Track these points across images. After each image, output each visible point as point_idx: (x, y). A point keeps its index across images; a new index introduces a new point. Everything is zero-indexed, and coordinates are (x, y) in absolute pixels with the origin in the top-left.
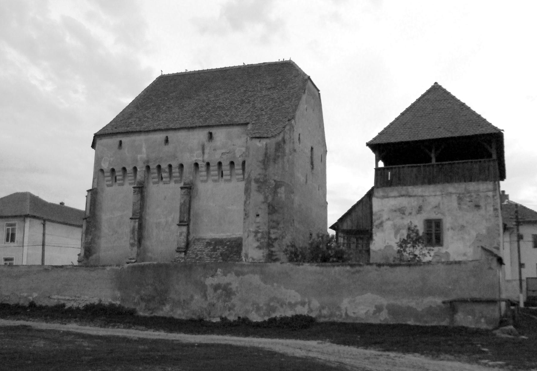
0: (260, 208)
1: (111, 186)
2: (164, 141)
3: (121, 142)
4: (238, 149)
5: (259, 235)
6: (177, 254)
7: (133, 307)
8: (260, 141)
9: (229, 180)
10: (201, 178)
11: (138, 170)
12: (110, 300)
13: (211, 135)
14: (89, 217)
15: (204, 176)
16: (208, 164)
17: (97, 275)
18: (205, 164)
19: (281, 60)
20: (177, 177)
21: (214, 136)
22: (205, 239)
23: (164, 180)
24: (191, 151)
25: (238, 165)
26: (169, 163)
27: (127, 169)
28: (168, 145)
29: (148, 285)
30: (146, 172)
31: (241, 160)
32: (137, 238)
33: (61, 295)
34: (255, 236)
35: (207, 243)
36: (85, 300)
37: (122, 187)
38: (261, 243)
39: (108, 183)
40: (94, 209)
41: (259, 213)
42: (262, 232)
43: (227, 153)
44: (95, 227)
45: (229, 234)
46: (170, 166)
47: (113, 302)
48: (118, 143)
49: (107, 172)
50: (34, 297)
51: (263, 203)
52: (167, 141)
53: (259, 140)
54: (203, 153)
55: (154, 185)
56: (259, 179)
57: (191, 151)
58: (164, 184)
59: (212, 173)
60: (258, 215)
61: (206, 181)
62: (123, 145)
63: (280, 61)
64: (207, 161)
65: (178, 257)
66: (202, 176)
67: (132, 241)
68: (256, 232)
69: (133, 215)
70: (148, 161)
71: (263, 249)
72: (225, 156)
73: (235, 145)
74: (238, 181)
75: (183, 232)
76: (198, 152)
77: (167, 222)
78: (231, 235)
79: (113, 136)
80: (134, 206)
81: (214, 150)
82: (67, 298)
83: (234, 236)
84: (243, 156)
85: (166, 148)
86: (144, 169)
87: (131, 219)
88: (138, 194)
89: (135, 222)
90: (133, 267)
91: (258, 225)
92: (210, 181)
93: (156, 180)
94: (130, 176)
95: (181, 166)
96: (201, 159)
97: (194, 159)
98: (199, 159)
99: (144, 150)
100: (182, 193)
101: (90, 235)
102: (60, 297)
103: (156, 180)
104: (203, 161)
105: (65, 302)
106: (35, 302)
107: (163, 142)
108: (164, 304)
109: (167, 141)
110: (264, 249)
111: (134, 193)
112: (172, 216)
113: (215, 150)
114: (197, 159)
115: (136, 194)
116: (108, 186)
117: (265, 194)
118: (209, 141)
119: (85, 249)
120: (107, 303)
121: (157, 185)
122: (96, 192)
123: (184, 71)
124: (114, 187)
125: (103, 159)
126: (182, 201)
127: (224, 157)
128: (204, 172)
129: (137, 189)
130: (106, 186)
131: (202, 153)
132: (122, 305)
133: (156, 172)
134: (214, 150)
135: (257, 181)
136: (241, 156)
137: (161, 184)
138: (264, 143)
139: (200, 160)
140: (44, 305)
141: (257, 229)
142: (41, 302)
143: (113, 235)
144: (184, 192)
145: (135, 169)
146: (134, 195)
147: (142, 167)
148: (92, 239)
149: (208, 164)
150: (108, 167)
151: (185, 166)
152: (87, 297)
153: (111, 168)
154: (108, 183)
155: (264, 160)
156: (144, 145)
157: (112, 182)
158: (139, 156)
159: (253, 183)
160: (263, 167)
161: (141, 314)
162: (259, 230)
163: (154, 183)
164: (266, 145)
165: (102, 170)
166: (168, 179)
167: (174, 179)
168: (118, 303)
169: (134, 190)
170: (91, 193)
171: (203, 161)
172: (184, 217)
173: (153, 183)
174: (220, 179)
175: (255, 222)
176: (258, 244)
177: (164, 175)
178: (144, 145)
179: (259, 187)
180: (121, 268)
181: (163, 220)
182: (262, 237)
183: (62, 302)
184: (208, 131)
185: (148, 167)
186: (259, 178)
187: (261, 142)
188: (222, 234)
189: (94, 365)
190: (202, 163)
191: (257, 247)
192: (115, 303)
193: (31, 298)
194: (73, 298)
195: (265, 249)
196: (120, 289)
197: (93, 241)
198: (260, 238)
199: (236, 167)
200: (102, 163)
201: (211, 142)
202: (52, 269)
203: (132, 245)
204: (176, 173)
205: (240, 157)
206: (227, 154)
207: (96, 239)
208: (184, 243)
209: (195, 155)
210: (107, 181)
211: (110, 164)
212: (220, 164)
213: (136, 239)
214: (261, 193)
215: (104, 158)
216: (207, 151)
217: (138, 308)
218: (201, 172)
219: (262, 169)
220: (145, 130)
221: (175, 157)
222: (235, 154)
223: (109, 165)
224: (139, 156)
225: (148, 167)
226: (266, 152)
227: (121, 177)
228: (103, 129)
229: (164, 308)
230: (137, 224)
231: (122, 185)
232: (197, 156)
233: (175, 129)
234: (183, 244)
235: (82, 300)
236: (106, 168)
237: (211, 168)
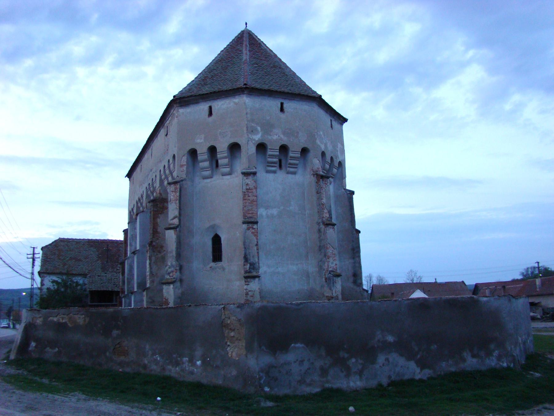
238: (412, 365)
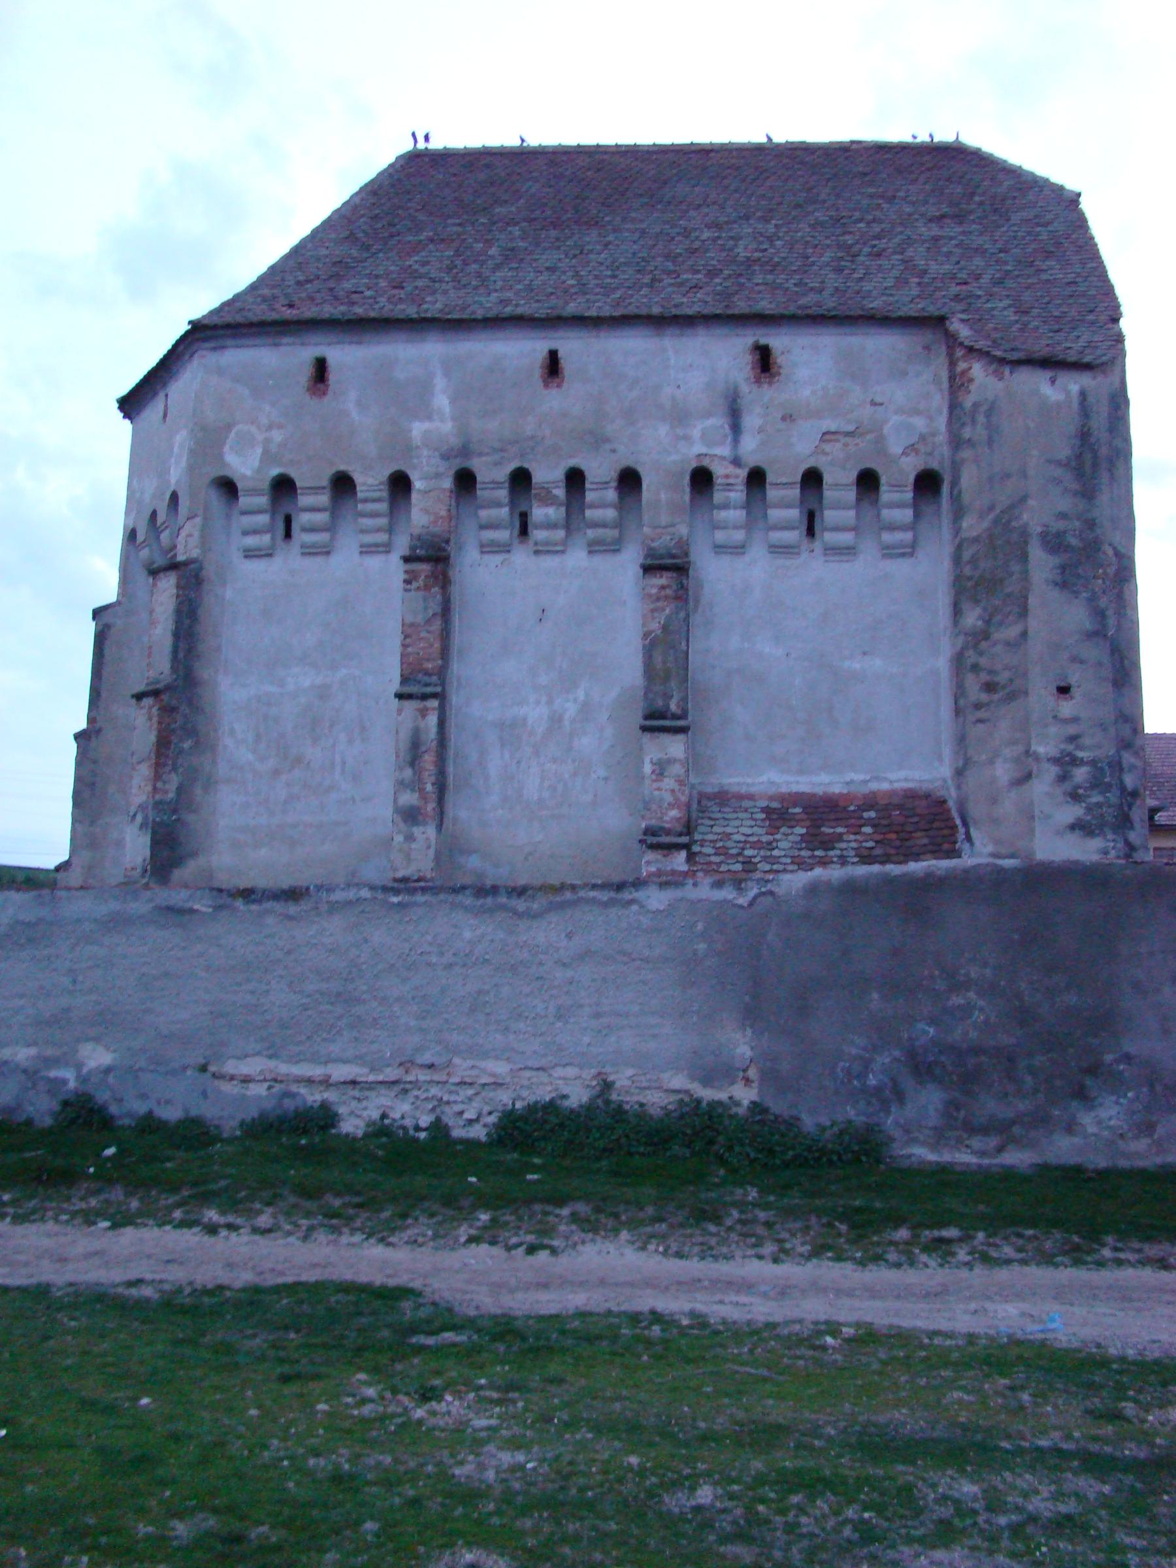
0: (1075, 659)
2: (542, 367)
3: (321, 369)
4: (895, 419)
5: (1081, 774)
6: (650, 856)
7: (853, 1113)
9: (848, 548)
10: (720, 536)
11: (418, 484)
12: (678, 1081)
13: (764, 361)
15: (736, 527)
16: (757, 478)
17: (569, 936)
18: (743, 473)
19: (923, 138)
20: (604, 525)
21: (779, 358)
22: (751, 797)
23: (538, 535)
24: (679, 416)
25: (897, 486)
26: (573, 462)
27: (358, 478)
28: (559, 386)
29: (958, 986)
31: (911, 467)
32: (433, 784)
33: (295, 1060)
34: (1063, 778)
35: (767, 810)
36: (484, 1085)
37: (319, 560)
38: (1089, 809)
39: (251, 541)
42: (1093, 763)
44: (191, 732)
45: (858, 777)
46: (575, 479)
47: (708, 1094)
48: (308, 371)
49: (255, 492)
50: (85, 1070)
51: (1092, 635)
53: (1048, 374)
55: (486, 557)
56: (1060, 535)
58: (537, 552)
59: (775, 514)
60: (1064, 690)
61: (739, 549)
62: (333, 377)
63: (918, 140)
65: (659, 870)
67: (409, 798)
68: (1066, 762)
69: (405, 680)
70: (465, 451)
71: (1102, 834)
72: (838, 445)
73: (882, 404)
75: (671, 761)
76: (709, 422)
77: (556, 720)
78: (865, 782)
79: (282, 334)
80: (408, 641)
81: (784, 419)
82: (340, 1072)
83: (885, 786)
84: (917, 452)
85: (553, 400)
88: (427, 588)
89: (423, 713)
90: (850, 888)
91: (1072, 730)
92: (758, 552)
93: (503, 535)
95: (629, 480)
96: (725, 451)
98: (718, 451)
99: (442, 402)
101: (174, 769)
102: (284, 1068)
103: (503, 535)
104: (736, 462)
105: (331, 1096)
106: (102, 1096)
107: (537, 373)
108: (1082, 1095)
109: (553, 366)
110: (1105, 836)
112: (581, 694)
113: (788, 418)
114: (704, 450)
115: (418, 588)
116: (250, 554)
117: (1093, 599)
118: (758, 381)
119: (154, 833)
120: (656, 1101)
121: (498, 558)
122: (197, 577)
123: (513, 142)
124: (277, 563)
125: (232, 435)
127: (835, 449)
128: (735, 508)
129: (424, 568)
130: (236, 557)
132: (778, 1107)
134: (784, 419)
135: (1054, 543)
136: (911, 449)
137: (521, 557)
138: (1074, 388)
139: (723, 458)
140: (171, 1114)
141: (1070, 747)
143: (276, 773)
144: (663, 587)
145: (400, 484)
146: (406, 590)
147: (438, 476)
148: (180, 789)
149: (757, 478)
150: (259, 470)
151: (648, 482)
152: (501, 1068)
153: (275, 472)
154: (251, 541)
155: (1079, 457)
156: (440, 383)
158: (418, 429)
160: (1075, 486)
162: (1080, 754)
163: (488, 548)
164: (1083, 394)
166: (561, 534)
167: (591, 533)
168: (745, 1095)
169: (406, 572)
171: (736, 462)
173: (482, 546)
174: (805, 543)
175: (1055, 717)
176: (1076, 811)
177: (539, 513)
178: (440, 383)
179: (1063, 568)
180: (755, 898)
181: (535, 713)
182: (1096, 784)
183: (314, 1097)
184: (755, 339)
185: (465, 481)
188: (824, 778)
189: (1020, 1546)
190: (731, 470)
191: (1073, 827)
192: (722, 1096)
194: (391, 1073)
196: (751, 1015)
197: (182, 802)
198: (1086, 789)
199: (886, 494)
200: (227, 448)
202: (218, 908)
203: (411, 816)
204: (603, 505)
205: (903, 453)
206: (844, 440)
207: (198, 791)
208: (679, 808)
209: (696, 433)
210: (246, 533)
211: (268, 457)
212: (812, 479)
214: (1076, 594)
216: (751, 421)
218: (725, 506)
219: (1075, 494)
220: (449, 317)
221: (598, 441)
222: (880, 440)
223: (261, 461)
224: (418, 429)
226: (1083, 426)
227: (322, 518)
228: (226, 309)
229: (1087, 1120)
230: (432, 720)
232: (703, 436)
236: (249, 473)
237: (772, 494)
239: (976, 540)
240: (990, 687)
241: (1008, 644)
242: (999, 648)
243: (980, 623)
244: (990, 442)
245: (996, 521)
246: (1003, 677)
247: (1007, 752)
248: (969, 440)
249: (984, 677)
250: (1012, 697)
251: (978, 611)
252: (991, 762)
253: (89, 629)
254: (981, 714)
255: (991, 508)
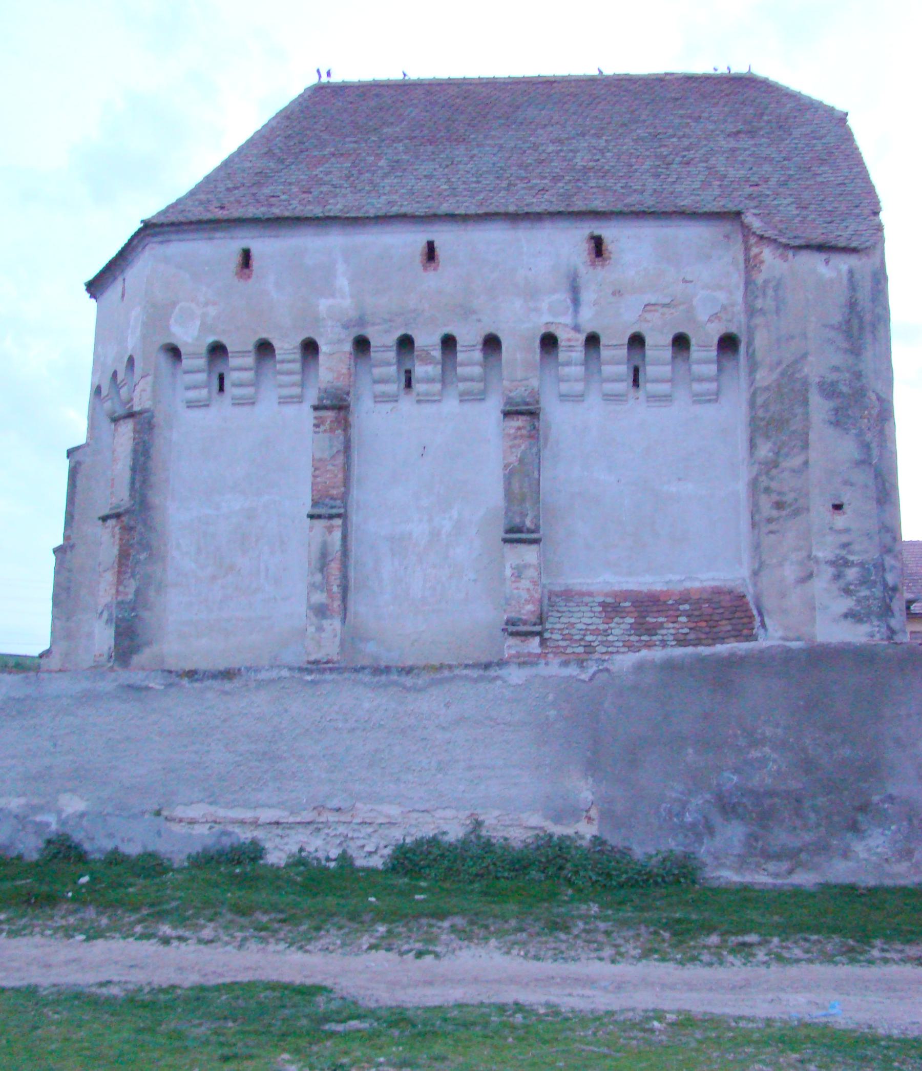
0: (847, 483)
1: (205, 405)
2: (421, 255)
5: (852, 574)
6: (511, 641)
7: (674, 844)
8: (827, 262)
10: (564, 388)
12: (535, 820)
13: (598, 247)
14: (127, 512)
15: (577, 380)
16: (593, 341)
17: (448, 705)
23: (418, 387)
24: (531, 293)
25: (704, 347)
27: (277, 344)
28: (435, 269)
30: (352, 357)
33: (230, 805)
38: (858, 601)
39: (193, 395)
40: (144, 482)
41: (845, 499)
42: (861, 564)
43: (664, 306)
44: (146, 546)
47: (558, 830)
48: (237, 259)
52: (431, 253)
53: (823, 256)
54: (576, 302)
55: (379, 406)
56: (833, 384)
57: (531, 293)
58: (419, 402)
60: (838, 507)
61: (579, 398)
62: (255, 263)
63: (719, 72)
64: (589, 331)
65: (518, 652)
66: (568, 381)
67: (319, 597)
68: (840, 564)
70: (361, 322)
71: (869, 620)
72: (657, 315)
73: (691, 282)
74: (694, 402)
75: (526, 566)
77: (435, 534)
78: (681, 581)
79: (215, 230)
80: (317, 472)
81: (614, 294)
82: (267, 815)
83: (697, 585)
85: (431, 280)
86: (348, 347)
87: (311, 517)
88: (332, 430)
89: (330, 529)
90: (670, 666)
91: (844, 539)
92: (594, 399)
93: (392, 388)
94: (290, 373)
96: (568, 320)
97: (541, 322)
99: (343, 282)
100: (512, 431)
102: (222, 813)
103: (392, 388)
104: (577, 328)
105: (259, 834)
106: (78, 836)
109: (431, 253)
110: (871, 622)
111: (316, 426)
112: (455, 514)
114: (550, 319)
115: (325, 431)
116: (191, 405)
117: (860, 434)
122: (149, 423)
124: (213, 410)
126: (513, 459)
127: (655, 318)
128: (576, 365)
130: (181, 407)
131: (568, 300)
132: (615, 839)
133: (394, 361)
134: (614, 294)
135: (829, 390)
137: (406, 404)
138: (844, 268)
139: (566, 325)
140: (132, 849)
142: (111, 836)
143: (214, 578)
144: (519, 428)
145: (310, 348)
147: (340, 341)
148: (138, 592)
149: (593, 341)
152: (394, 811)
153: (211, 339)
154: (193, 395)
155: (848, 322)
157: (209, 392)
158: (324, 304)
159: (815, 399)
160: (846, 345)
161: (730, 876)
163: (380, 399)
164: (851, 272)
165: (174, 352)
166: (437, 387)
167: (462, 386)
168: (587, 831)
170: (135, 425)
172: (523, 515)
173: (375, 397)
177: (420, 370)
178: (341, 268)
179: (836, 410)
180: (594, 674)
182: (864, 581)
183: (245, 835)
185: (362, 345)
186: (837, 382)
187: (830, 263)
190: (573, 335)
191: (846, 616)
192: (569, 831)
193: (52, 820)
194: (307, 816)
195: (876, 623)
196: (592, 767)
198: (856, 585)
199: (695, 353)
200: (172, 321)
201: (599, 268)
207: (152, 593)
208: (533, 603)
209: (544, 306)
210: (188, 388)
211: (205, 328)
212: (637, 341)
213: (335, 589)
214: (847, 431)
215: (178, 307)
216: (588, 296)
217: (703, 852)
218: (568, 364)
219: (846, 351)
220: (348, 215)
221: (467, 312)
224: (324, 304)
225: (362, 345)
228: (171, 210)
229: (859, 848)
231: (251, 402)
233: (465, 218)
234: (530, 607)
235: (363, 823)
236: (190, 340)
237: (605, 353)
238: (286, 813)
239: (767, 388)
240: (779, 505)
241: (793, 471)
242: (786, 474)
243: (771, 454)
244: (778, 311)
245: (782, 374)
246: (789, 497)
247: (794, 557)
248: (761, 309)
249: (775, 497)
250: (797, 512)
251: (769, 445)
252: (781, 564)
253: (64, 466)
254: (773, 527)
255: (779, 363)
